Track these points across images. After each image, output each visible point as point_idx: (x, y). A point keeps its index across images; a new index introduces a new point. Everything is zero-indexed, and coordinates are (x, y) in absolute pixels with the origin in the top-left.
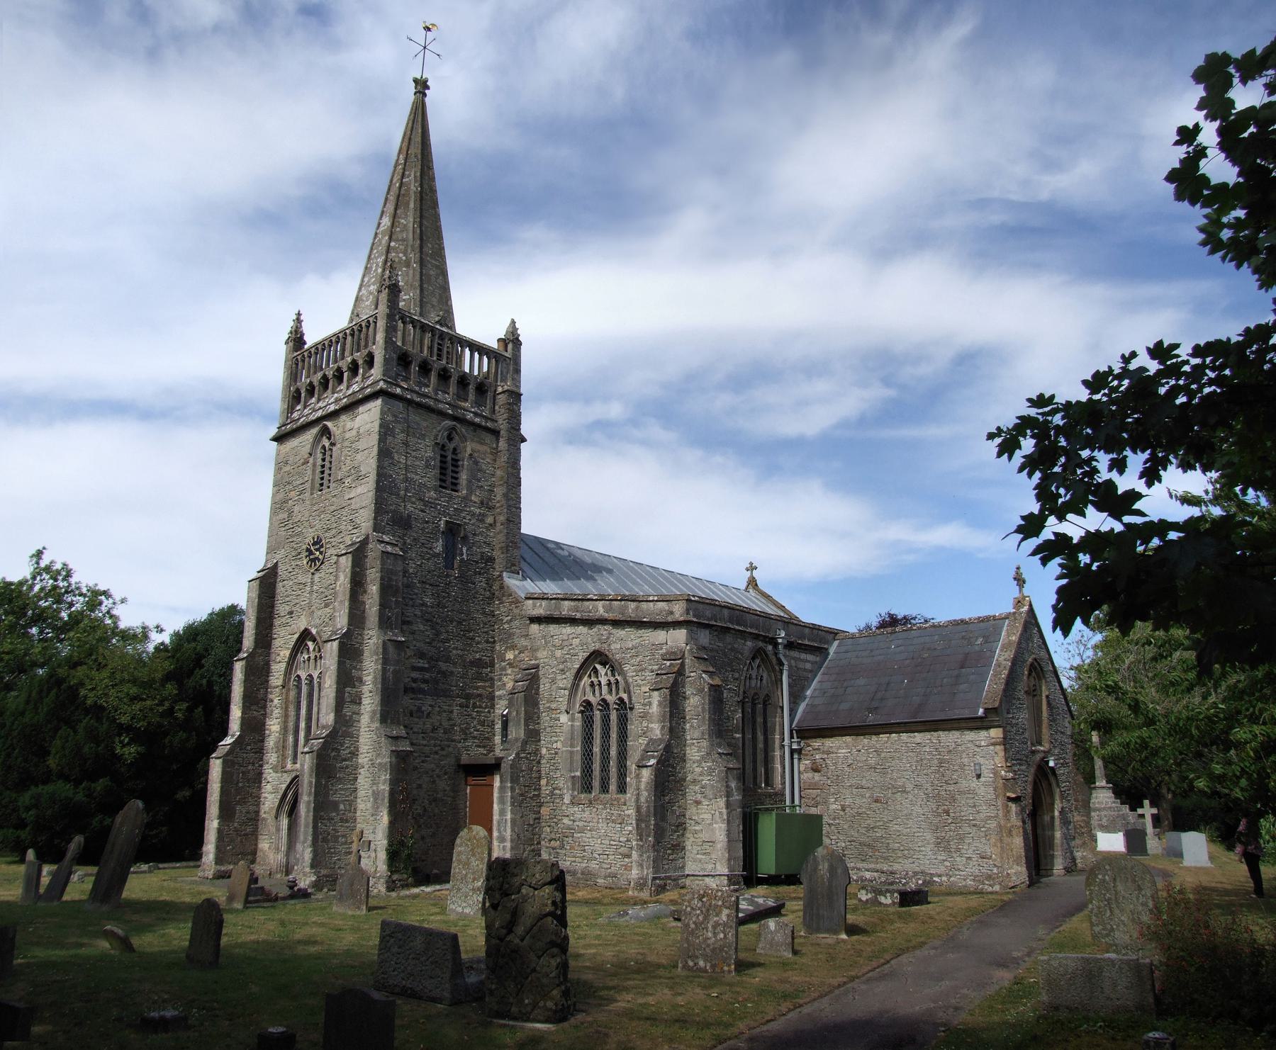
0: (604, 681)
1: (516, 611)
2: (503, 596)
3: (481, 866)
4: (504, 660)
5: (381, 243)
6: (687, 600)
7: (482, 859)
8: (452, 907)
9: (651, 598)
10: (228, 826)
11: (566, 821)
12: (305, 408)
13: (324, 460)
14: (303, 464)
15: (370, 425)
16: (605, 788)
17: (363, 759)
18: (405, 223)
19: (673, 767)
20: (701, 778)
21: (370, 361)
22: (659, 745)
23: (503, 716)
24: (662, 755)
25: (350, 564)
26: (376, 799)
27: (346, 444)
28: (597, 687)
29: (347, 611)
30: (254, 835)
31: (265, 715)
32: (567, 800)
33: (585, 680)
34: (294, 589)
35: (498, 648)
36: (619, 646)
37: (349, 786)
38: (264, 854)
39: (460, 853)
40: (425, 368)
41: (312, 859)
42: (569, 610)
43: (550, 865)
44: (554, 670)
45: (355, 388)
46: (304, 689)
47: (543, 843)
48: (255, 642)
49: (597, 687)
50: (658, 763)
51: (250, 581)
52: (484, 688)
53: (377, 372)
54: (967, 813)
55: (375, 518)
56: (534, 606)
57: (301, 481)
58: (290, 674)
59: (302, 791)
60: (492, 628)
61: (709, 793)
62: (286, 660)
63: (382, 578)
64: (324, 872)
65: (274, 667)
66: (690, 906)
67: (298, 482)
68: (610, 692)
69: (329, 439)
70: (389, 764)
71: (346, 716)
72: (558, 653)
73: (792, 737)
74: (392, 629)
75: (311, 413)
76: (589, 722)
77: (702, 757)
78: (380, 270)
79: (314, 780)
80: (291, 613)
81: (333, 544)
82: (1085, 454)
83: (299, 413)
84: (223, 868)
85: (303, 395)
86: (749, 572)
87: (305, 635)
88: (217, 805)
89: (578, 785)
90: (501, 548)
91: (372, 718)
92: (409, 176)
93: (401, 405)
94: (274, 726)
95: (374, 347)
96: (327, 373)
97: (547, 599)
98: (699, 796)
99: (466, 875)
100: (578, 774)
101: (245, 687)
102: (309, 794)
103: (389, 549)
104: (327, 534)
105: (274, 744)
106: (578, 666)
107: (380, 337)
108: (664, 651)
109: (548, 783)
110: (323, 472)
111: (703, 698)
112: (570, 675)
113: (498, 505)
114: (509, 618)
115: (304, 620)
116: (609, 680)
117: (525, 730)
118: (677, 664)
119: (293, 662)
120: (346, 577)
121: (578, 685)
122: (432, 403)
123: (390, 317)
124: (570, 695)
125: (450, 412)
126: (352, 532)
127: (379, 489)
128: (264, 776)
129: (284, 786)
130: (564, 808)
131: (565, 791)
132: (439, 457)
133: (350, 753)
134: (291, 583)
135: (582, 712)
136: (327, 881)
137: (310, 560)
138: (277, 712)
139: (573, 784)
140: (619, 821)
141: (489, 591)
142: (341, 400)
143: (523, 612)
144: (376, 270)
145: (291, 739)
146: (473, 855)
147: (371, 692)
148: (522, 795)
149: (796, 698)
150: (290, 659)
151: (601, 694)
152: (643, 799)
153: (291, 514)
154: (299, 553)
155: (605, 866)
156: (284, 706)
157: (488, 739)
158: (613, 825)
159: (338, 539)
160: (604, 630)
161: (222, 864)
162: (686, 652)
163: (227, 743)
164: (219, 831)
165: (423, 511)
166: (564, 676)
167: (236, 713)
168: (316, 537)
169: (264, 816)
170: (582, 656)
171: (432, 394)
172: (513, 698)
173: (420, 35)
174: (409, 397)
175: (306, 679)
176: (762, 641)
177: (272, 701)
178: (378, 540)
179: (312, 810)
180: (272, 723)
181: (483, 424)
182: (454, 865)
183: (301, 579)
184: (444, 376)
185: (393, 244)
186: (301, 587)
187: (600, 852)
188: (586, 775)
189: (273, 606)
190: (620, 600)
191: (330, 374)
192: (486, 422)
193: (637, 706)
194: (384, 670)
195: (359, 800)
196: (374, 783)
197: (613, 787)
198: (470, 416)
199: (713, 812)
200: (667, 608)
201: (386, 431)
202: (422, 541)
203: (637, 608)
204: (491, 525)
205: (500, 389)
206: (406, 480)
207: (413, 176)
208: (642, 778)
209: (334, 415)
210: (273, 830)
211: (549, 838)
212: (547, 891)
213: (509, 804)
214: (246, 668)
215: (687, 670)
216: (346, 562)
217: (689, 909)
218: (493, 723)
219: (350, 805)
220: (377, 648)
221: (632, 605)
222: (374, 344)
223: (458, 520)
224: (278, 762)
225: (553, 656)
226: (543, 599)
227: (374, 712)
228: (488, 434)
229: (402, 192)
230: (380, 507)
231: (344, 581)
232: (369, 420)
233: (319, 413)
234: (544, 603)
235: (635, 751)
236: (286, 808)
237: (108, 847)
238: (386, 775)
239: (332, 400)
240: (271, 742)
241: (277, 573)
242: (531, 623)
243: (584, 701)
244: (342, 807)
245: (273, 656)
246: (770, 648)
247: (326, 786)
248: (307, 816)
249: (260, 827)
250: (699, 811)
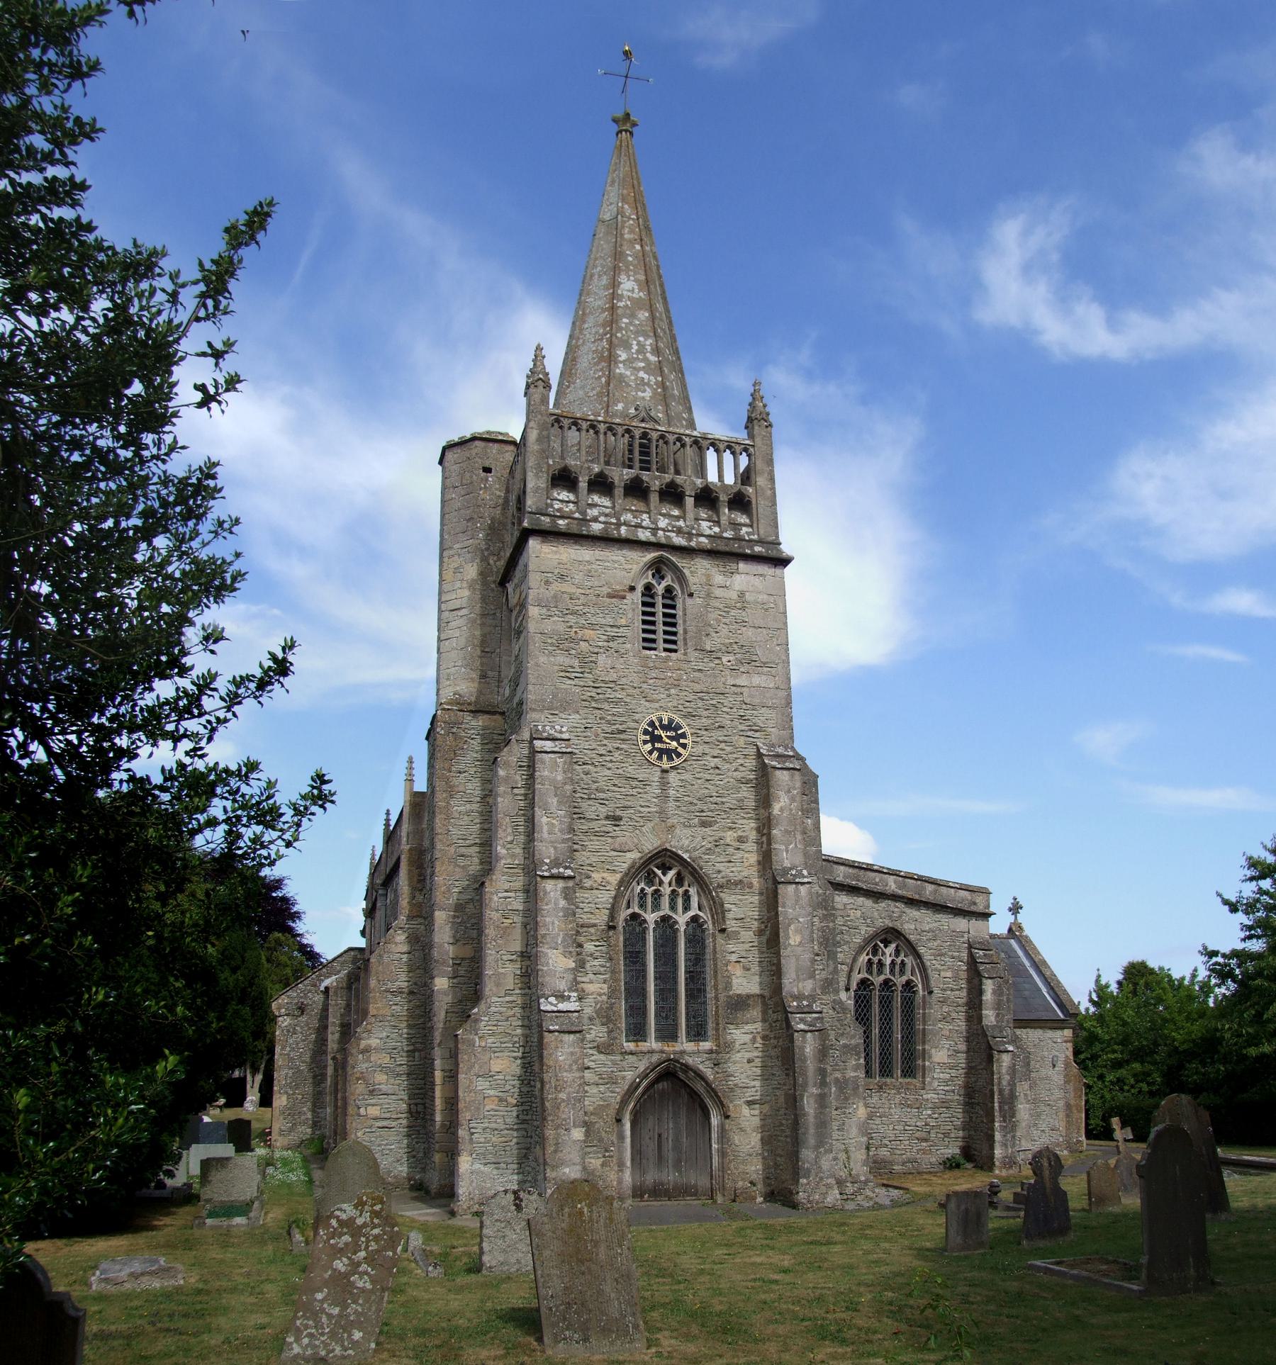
15: (765, 596)
36: (913, 927)
54: (1044, 1095)
82: (29, 704)
155: (899, 1152)
173: (622, 67)
193: (936, 990)
203: (936, 891)
221: (930, 888)
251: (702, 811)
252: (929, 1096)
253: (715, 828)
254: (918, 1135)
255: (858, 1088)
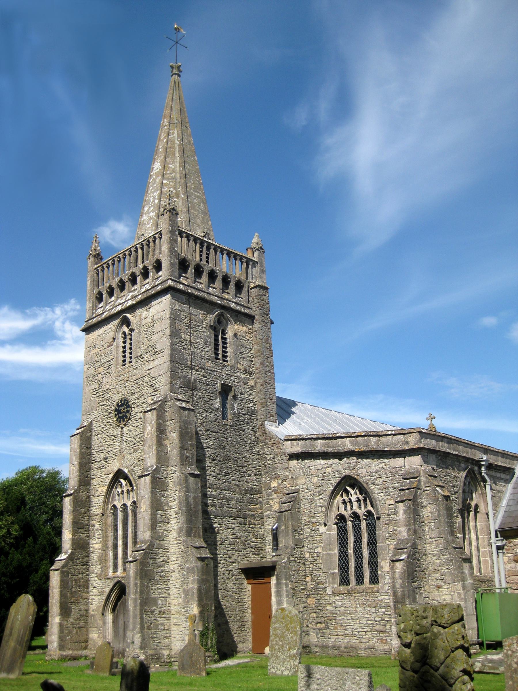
0: (354, 498)
1: (278, 450)
2: (266, 439)
3: (295, 638)
4: (269, 488)
5: (155, 182)
6: (419, 432)
7: (296, 632)
8: (272, 670)
9: (389, 433)
10: (67, 621)
11: (329, 607)
12: (106, 305)
13: (125, 342)
14: (108, 347)
16: (360, 580)
17: (173, 565)
18: (173, 167)
19: (418, 560)
20: (440, 568)
21: (158, 266)
22: (407, 544)
23: (273, 530)
24: (411, 551)
25: (155, 417)
26: (186, 595)
27: (143, 328)
28: (348, 504)
29: (155, 453)
30: (86, 627)
31: (89, 537)
32: (329, 591)
33: (339, 499)
34: (107, 440)
35: (264, 479)
36: (365, 471)
37: (164, 586)
38: (94, 642)
39: (275, 629)
40: (198, 271)
41: (141, 643)
42: (321, 446)
43: (456, 607)
44: (312, 492)
45: (148, 287)
46: (120, 515)
47: (310, 625)
48: (79, 482)
49: (348, 504)
50: (408, 557)
51: (72, 436)
52: (255, 509)
53: (164, 274)
55: (171, 383)
56: (292, 445)
57: (108, 359)
58: (108, 504)
59: (129, 590)
60: (258, 464)
61: (448, 579)
62: (104, 494)
63: (180, 427)
64: (150, 652)
65: (94, 500)
66: (510, 650)
67: (105, 361)
68: (346, 509)
69: (128, 326)
70: (196, 568)
71: (159, 532)
72: (315, 480)
73: (497, 537)
74: (190, 465)
75: (112, 308)
76: (343, 531)
77: (441, 551)
78: (157, 201)
79: (139, 582)
80: (105, 458)
81: (138, 404)
83: (102, 309)
84: (65, 653)
85: (104, 296)
86: (429, 421)
87: (119, 474)
88: (58, 605)
89: (337, 580)
90: (262, 403)
91: (179, 534)
92: (173, 133)
93: (184, 297)
94: (96, 545)
95: (161, 255)
96: (123, 278)
97: (303, 439)
98: (440, 582)
99: (282, 646)
100: (337, 571)
101: (73, 515)
102: (136, 593)
103: (184, 405)
104: (132, 397)
105: (98, 558)
106: (332, 488)
107: (165, 248)
108: (403, 472)
109: (312, 579)
110: (124, 352)
111: (438, 506)
112: (326, 496)
113: (257, 371)
114: (272, 455)
115: (117, 463)
116: (358, 498)
117: (293, 539)
118: (416, 481)
119: (110, 496)
120: (152, 427)
121: (333, 503)
122: (205, 295)
123: (172, 232)
124: (327, 511)
125: (219, 302)
126: (153, 394)
127: (173, 360)
128: (91, 582)
129: (108, 590)
130: (327, 598)
131: (327, 585)
132: (213, 336)
133: (163, 561)
134: (104, 436)
135: (336, 524)
136: (153, 659)
137: (119, 417)
138: (98, 534)
139: (334, 579)
140: (373, 606)
141: (255, 435)
142: (136, 296)
143: (283, 451)
144: (154, 201)
145: (111, 554)
146: (288, 630)
147: (177, 514)
148: (294, 589)
149: (496, 506)
150: (107, 493)
151: (352, 509)
152: (398, 586)
153: (100, 384)
154: (110, 413)
155: (364, 641)
156: (104, 529)
157: (261, 548)
158: (369, 608)
159: (141, 400)
160: (352, 460)
161: (64, 650)
162: (421, 472)
163: (62, 558)
164: (61, 625)
165: (204, 377)
166: (321, 497)
167: (67, 536)
168: (123, 400)
169: (92, 613)
170: (335, 481)
171: (205, 289)
172: (281, 515)
174: (189, 291)
175: (121, 507)
176: (471, 463)
177: (94, 526)
178: (175, 399)
179: (138, 605)
180: (95, 542)
181: (243, 311)
182: (271, 638)
183: (112, 432)
184: (212, 276)
185: (165, 182)
186: (113, 438)
187: (359, 630)
188: (343, 572)
189: (90, 455)
190: (364, 436)
191: (126, 278)
192: (245, 310)
193: (383, 516)
194: (187, 497)
195: (172, 597)
196: (184, 582)
197: (367, 579)
198: (233, 305)
199: (452, 593)
200: (403, 439)
201: (174, 318)
202: (206, 399)
203: (378, 441)
204: (252, 386)
205: (252, 285)
206: (192, 353)
207: (176, 133)
208: (396, 569)
209: (132, 309)
210: (101, 623)
211: (315, 621)
212: (456, 628)
213: (285, 596)
214: (74, 501)
215: (423, 486)
216: (151, 416)
217: (510, 652)
218: (263, 538)
219: (166, 600)
220: (180, 480)
221: (374, 439)
222: (160, 253)
223: (229, 383)
224: (102, 571)
225: (310, 482)
226: (299, 440)
227: (180, 530)
228: (246, 319)
229: (169, 145)
230: (174, 374)
231: (150, 430)
232: (160, 310)
233: (120, 308)
234: (300, 442)
235: (384, 550)
236: (110, 606)
237: (7, 631)
238: (194, 577)
239: (129, 297)
240: (94, 557)
241: (92, 429)
242: (289, 460)
243: (338, 515)
244: (160, 602)
245: (93, 492)
246: (476, 468)
247: (148, 587)
248: (135, 610)
249: (90, 621)
250: (441, 593)
251: (135, 444)
252: (382, 598)
253: (138, 452)
254: (377, 628)
255: (194, 595)
